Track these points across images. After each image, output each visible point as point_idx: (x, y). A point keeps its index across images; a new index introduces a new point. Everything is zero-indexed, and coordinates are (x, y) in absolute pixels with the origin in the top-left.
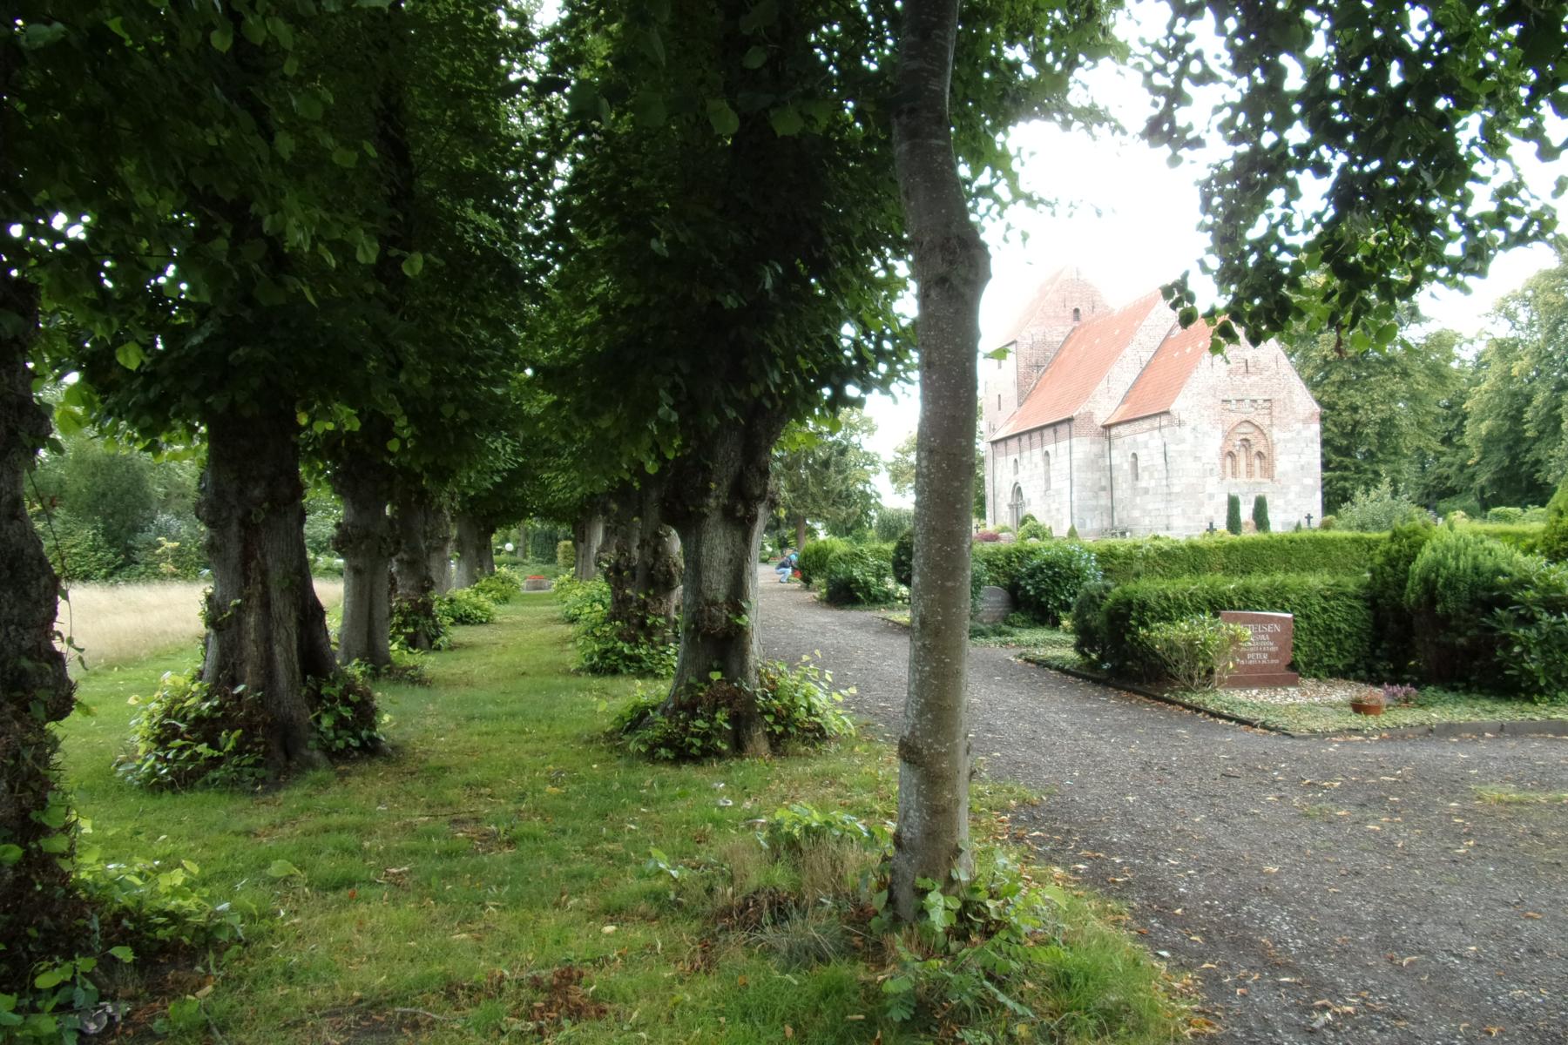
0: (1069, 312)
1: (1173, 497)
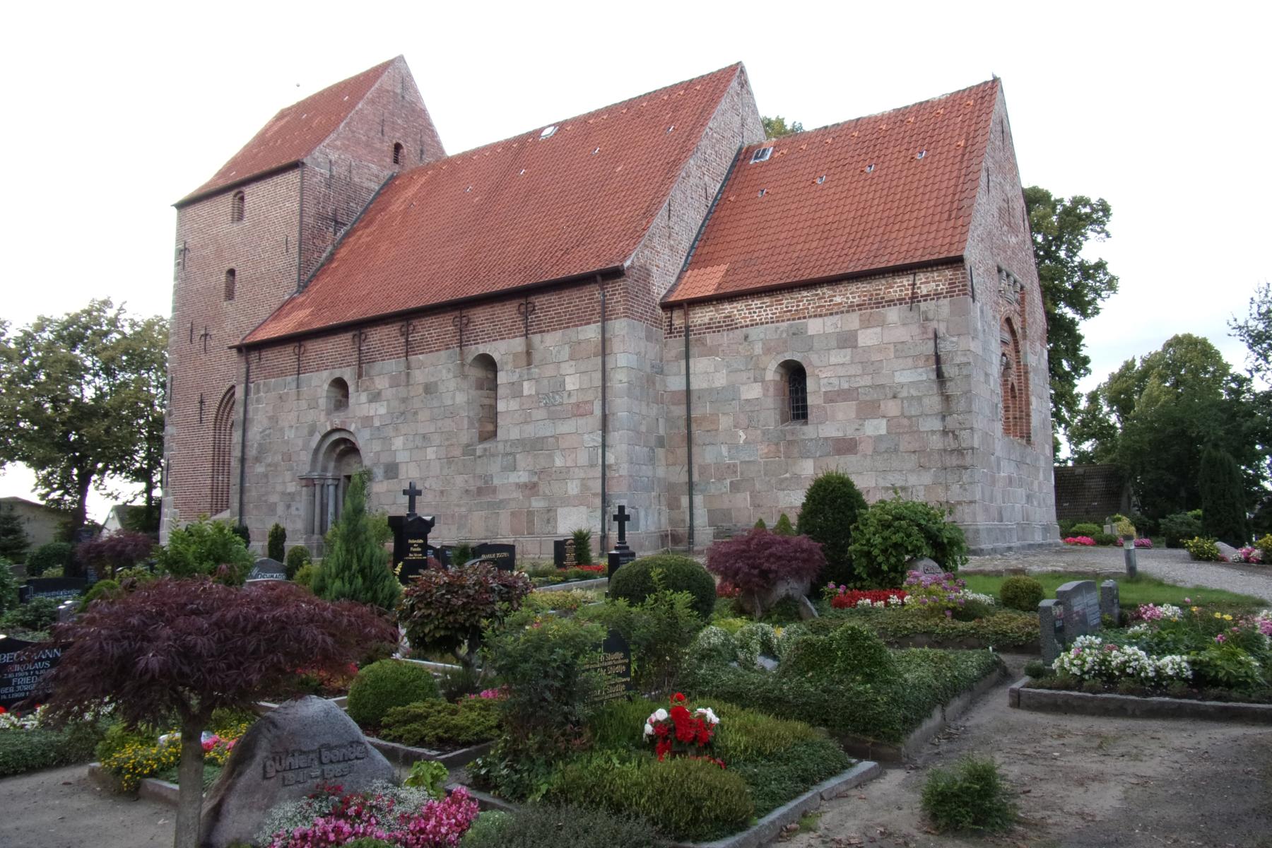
0: (388, 147)
1: (968, 460)
